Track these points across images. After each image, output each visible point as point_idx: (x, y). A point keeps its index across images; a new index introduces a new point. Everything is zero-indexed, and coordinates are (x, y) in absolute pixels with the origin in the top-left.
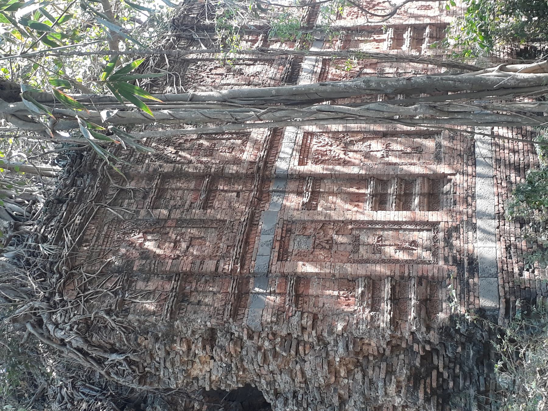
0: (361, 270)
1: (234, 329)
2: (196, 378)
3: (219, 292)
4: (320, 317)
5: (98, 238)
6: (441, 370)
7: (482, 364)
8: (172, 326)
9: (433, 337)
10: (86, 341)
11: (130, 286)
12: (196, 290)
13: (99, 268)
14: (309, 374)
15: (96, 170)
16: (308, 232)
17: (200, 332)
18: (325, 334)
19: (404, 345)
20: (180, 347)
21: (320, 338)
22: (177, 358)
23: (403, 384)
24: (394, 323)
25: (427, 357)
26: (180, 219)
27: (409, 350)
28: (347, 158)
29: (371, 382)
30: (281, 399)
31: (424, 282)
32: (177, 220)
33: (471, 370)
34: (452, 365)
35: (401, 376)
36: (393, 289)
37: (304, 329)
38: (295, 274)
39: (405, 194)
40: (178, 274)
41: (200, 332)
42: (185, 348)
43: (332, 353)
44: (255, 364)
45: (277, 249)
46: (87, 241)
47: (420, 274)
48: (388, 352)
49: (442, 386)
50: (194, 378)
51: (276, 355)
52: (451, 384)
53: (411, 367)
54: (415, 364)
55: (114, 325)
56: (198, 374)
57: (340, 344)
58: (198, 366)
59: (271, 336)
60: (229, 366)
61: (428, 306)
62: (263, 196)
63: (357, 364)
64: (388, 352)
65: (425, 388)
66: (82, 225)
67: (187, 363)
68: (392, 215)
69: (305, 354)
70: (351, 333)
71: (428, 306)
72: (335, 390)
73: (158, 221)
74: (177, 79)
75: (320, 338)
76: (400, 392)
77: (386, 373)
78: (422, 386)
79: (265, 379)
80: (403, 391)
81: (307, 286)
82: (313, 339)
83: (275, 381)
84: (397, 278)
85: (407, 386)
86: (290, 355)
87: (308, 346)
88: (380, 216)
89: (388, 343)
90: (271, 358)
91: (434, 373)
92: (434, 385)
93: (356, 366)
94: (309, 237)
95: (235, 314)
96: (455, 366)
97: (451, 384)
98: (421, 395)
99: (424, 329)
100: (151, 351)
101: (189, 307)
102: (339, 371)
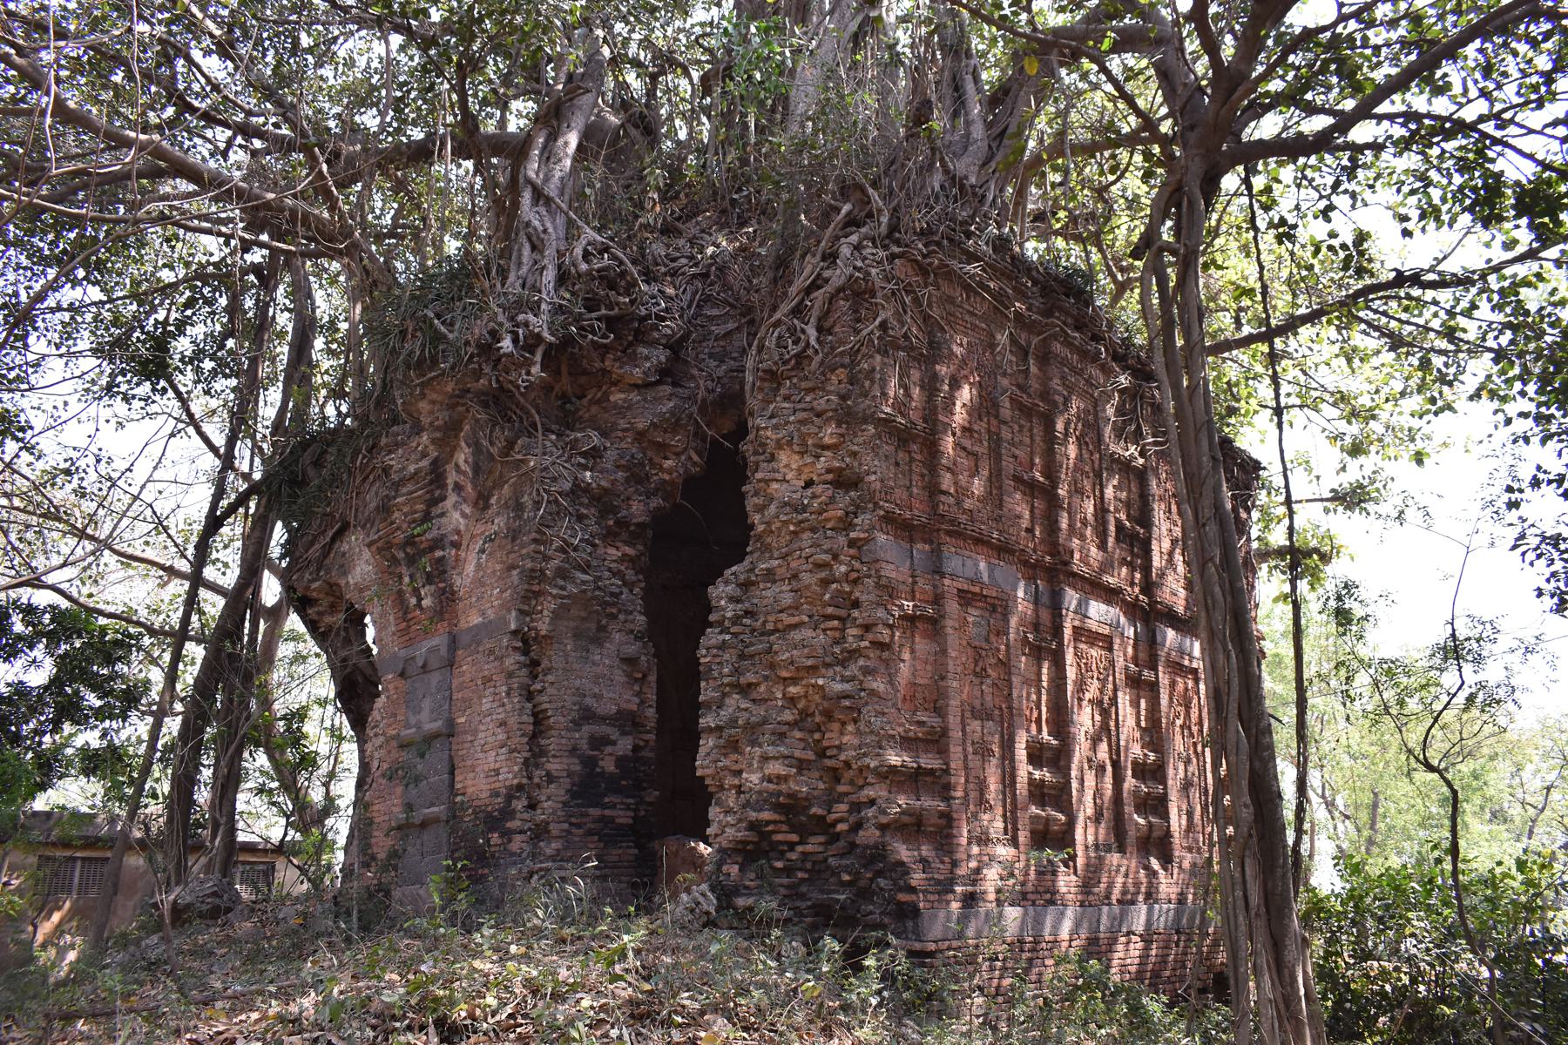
0: (953, 721)
1: (862, 519)
2: (772, 458)
3: (911, 495)
4: (885, 655)
5: (972, 314)
6: (800, 848)
7: (816, 915)
8: (865, 421)
9: (868, 835)
10: (840, 290)
11: (914, 359)
13: (935, 313)
14: (796, 635)
15: (1052, 315)
16: (993, 638)
17: (856, 464)
18: (861, 662)
19: (841, 788)
20: (829, 434)
21: (854, 654)
22: (814, 430)
23: (783, 787)
24: (890, 775)
25: (823, 826)
26: (999, 439)
27: (831, 799)
29: (782, 735)
30: (738, 592)
31: (943, 822)
32: (998, 435)
33: (802, 897)
34: (809, 866)
35: (797, 783)
36: (931, 772)
37: (867, 628)
38: (943, 617)
39: (1043, 795)
41: (856, 464)
42: (827, 440)
43: (830, 672)
44: (813, 550)
45: (972, 588)
46: (968, 297)
47: (955, 816)
48: (828, 763)
50: (772, 455)
51: (825, 583)
52: (779, 864)
55: (865, 332)
56: (779, 461)
57: (847, 687)
59: (855, 575)
60: (804, 509)
61: (912, 827)
63: (805, 714)
64: (828, 763)
65: (775, 822)
66: (987, 289)
67: (804, 444)
68: (1024, 770)
69: (824, 630)
71: (912, 827)
72: (766, 678)
73: (996, 405)
74: (1160, 444)
75: (854, 654)
76: (770, 781)
77: (800, 760)
78: (776, 817)
80: (772, 786)
81: (925, 635)
82: (851, 643)
83: (774, 582)
85: (780, 793)
86: (824, 606)
87: (837, 634)
88: (1021, 753)
89: (847, 764)
91: (794, 837)
92: (779, 837)
93: (800, 714)
94: (987, 640)
95: (889, 519)
96: (806, 871)
97: (779, 864)
98: (766, 815)
99: (884, 820)
101: (892, 448)
102: (795, 684)
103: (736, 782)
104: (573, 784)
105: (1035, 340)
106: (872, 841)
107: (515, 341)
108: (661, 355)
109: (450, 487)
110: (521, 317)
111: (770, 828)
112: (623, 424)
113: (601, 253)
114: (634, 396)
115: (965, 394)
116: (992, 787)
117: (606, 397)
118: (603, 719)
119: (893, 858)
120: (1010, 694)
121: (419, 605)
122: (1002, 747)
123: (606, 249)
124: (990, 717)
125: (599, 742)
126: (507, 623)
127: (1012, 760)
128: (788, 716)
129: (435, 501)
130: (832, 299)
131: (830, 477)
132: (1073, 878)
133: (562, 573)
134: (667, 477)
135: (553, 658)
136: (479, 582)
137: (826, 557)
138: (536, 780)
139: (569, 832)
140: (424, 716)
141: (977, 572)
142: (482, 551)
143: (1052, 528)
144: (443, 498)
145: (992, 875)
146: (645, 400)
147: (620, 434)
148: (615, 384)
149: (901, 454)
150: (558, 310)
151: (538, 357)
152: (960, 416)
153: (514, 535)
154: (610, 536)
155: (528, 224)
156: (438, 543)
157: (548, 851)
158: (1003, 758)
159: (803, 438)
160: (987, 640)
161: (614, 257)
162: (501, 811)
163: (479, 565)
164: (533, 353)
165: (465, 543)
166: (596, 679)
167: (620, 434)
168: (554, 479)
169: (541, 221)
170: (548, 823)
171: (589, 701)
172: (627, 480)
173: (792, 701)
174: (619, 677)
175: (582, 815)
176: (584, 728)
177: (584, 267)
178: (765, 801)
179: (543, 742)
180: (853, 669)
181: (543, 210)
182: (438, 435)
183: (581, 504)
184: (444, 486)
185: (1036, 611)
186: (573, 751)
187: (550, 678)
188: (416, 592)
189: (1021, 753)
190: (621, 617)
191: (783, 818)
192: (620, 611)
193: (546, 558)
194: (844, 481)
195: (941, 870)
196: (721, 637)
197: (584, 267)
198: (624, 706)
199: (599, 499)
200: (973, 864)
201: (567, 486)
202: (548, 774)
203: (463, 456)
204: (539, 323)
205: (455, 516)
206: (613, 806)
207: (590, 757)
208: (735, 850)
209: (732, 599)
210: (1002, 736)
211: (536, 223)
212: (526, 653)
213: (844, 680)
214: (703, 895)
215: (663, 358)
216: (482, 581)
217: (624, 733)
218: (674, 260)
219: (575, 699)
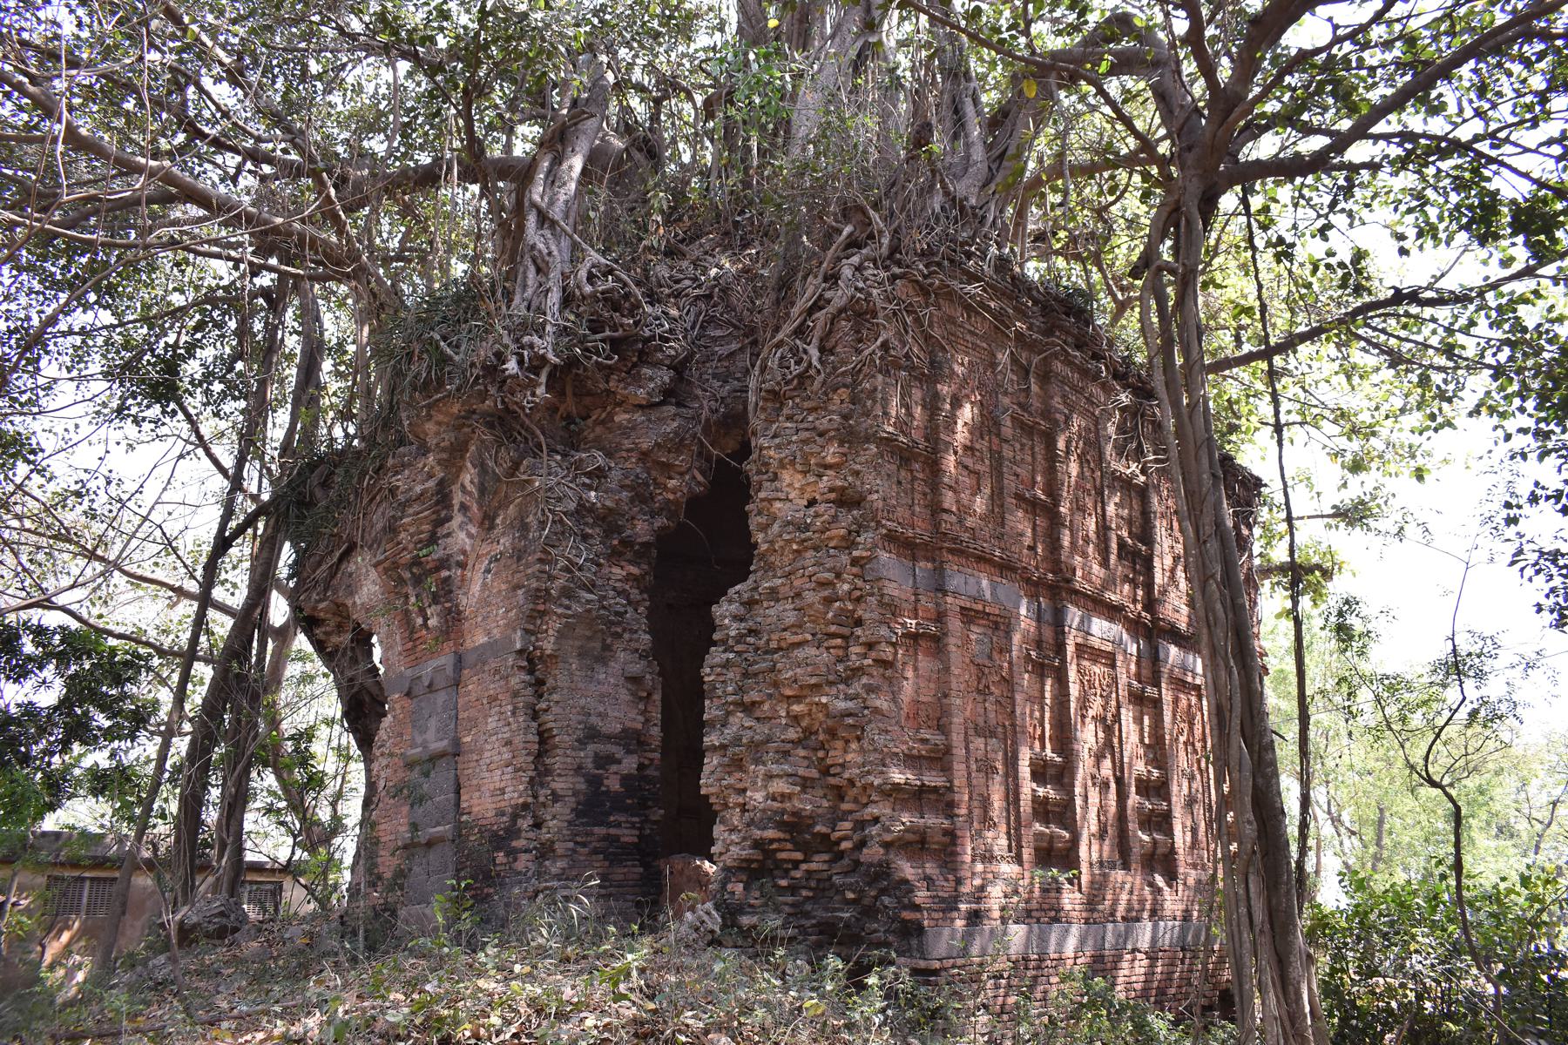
0: (957, 739)
2: (775, 478)
4: (889, 673)
6: (804, 866)
7: (821, 933)
8: (867, 440)
9: (873, 853)
10: (841, 311)
12: (914, 479)
13: (936, 333)
14: (800, 654)
16: (996, 656)
18: (864, 680)
19: (845, 806)
20: (832, 453)
21: (858, 672)
22: (816, 449)
23: (788, 805)
24: (894, 792)
25: (827, 844)
26: (1001, 457)
27: (835, 818)
28: (1088, 720)
29: (786, 754)
30: (742, 611)
31: (947, 839)
33: (807, 915)
34: (813, 884)
35: (801, 800)
36: (935, 789)
37: (870, 646)
38: (945, 634)
39: (1047, 812)
40: (935, 451)
42: (830, 460)
43: (834, 691)
45: (975, 607)
46: (969, 317)
47: (959, 833)
48: (832, 781)
49: (777, 867)
50: (776, 474)
51: (828, 601)
52: (784, 883)
53: (813, 818)
54: (815, 824)
55: (867, 352)
57: (850, 704)
58: (798, 480)
59: (858, 593)
60: (807, 528)
61: (916, 845)
62: (1035, 588)
63: (808, 732)
64: (832, 781)
65: (779, 840)
66: (988, 309)
67: (806, 463)
68: (1027, 787)
70: (870, 721)
71: (916, 845)
73: (997, 424)
75: (858, 672)
76: (774, 799)
77: (805, 779)
78: (781, 835)
79: (783, 585)
80: (776, 805)
82: (855, 661)
83: (778, 600)
84: (948, 797)
85: (783, 812)
87: (841, 652)
88: (1025, 770)
89: (851, 782)
90: (826, 593)
91: (798, 856)
94: (990, 658)
95: (891, 537)
96: (810, 889)
97: (784, 883)
98: (770, 833)
99: (888, 838)
100: (826, 409)
101: (894, 467)
102: (799, 703)
103: (741, 800)
104: (578, 803)
105: (1036, 359)
106: (876, 859)
107: (520, 362)
108: (665, 376)
109: (456, 508)
110: (526, 339)
111: (774, 846)
112: (627, 444)
113: (605, 275)
114: (639, 417)
115: (967, 413)
116: (996, 805)
117: (610, 417)
118: (609, 738)
119: (897, 876)
120: (1013, 712)
121: (425, 625)
122: (1006, 764)
123: (611, 271)
124: (993, 734)
125: (604, 761)
126: (513, 642)
127: (1016, 778)
128: (792, 734)
129: (440, 522)
130: (834, 319)
131: (833, 496)
132: (1078, 895)
133: (567, 593)
134: (671, 497)
135: (559, 677)
136: (484, 602)
137: (830, 576)
138: (542, 799)
139: (574, 851)
140: (431, 735)
141: (980, 589)
142: (488, 571)
143: (1054, 545)
144: (449, 519)
145: (996, 892)
146: (649, 420)
147: (624, 454)
148: (620, 404)
149: (903, 473)
150: (563, 331)
151: (543, 379)
152: (961, 435)
153: (519, 555)
154: (615, 556)
155: (533, 247)
156: (443, 564)
157: (554, 870)
158: (1006, 775)
159: (806, 457)
160: (990, 658)
161: (618, 279)
162: (507, 830)
163: (484, 585)
164: (538, 375)
165: (470, 563)
166: (602, 697)
167: (624, 454)
168: (559, 500)
169: (546, 244)
170: (553, 842)
171: (594, 720)
172: (632, 500)
173: (795, 719)
174: (624, 695)
175: (587, 834)
176: (589, 747)
177: (588, 289)
178: (770, 819)
179: (548, 761)
180: (856, 688)
181: (548, 233)
182: (445, 456)
183: (586, 524)
184: (450, 507)
185: (1039, 628)
186: (579, 769)
187: (555, 697)
188: (422, 611)
189: (1025, 770)
190: (626, 636)
191: (788, 836)
192: (624, 630)
193: (551, 578)
194: (846, 500)
195: (945, 887)
196: (724, 656)
197: (588, 289)
198: (629, 724)
199: (604, 519)
200: (977, 882)
201: (572, 506)
202: (554, 793)
203: (468, 477)
204: (544, 345)
205: (461, 536)
206: (619, 825)
207: (595, 776)
208: (739, 868)
209: (738, 618)
210: (1006, 754)
211: (541, 246)
212: (531, 672)
213: (848, 698)
214: (708, 913)
215: (666, 379)
216: (487, 600)
217: (629, 752)
218: (678, 282)
219: (580, 718)
